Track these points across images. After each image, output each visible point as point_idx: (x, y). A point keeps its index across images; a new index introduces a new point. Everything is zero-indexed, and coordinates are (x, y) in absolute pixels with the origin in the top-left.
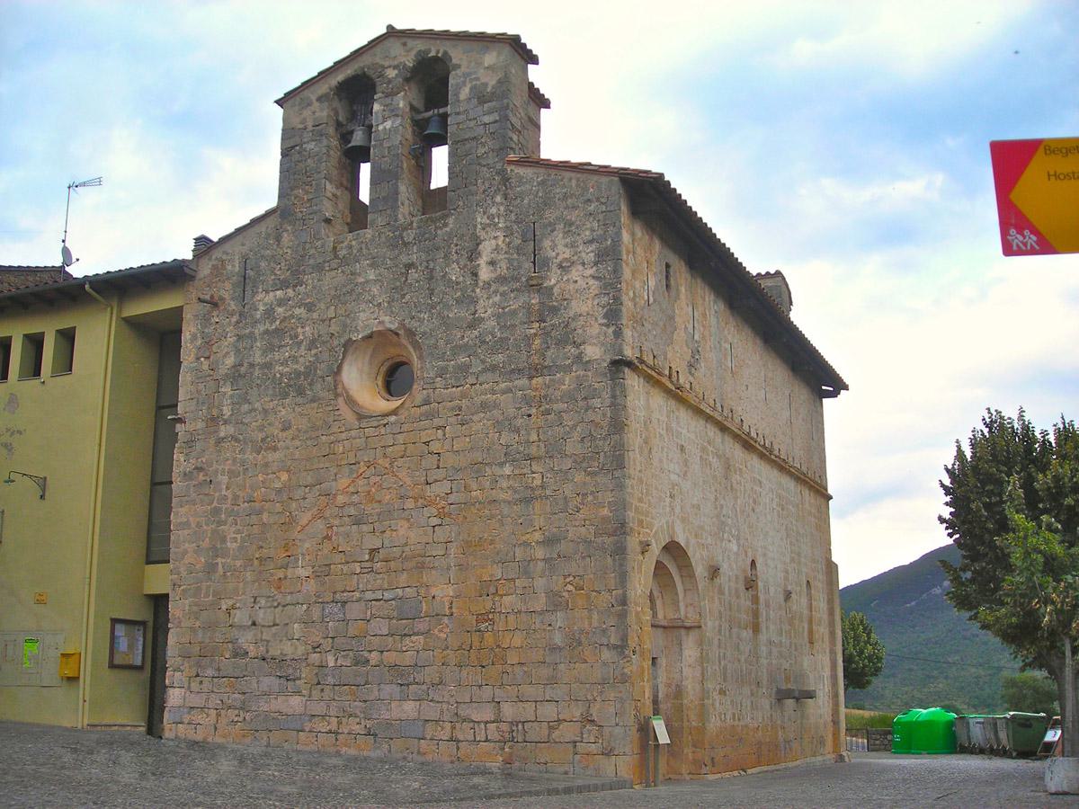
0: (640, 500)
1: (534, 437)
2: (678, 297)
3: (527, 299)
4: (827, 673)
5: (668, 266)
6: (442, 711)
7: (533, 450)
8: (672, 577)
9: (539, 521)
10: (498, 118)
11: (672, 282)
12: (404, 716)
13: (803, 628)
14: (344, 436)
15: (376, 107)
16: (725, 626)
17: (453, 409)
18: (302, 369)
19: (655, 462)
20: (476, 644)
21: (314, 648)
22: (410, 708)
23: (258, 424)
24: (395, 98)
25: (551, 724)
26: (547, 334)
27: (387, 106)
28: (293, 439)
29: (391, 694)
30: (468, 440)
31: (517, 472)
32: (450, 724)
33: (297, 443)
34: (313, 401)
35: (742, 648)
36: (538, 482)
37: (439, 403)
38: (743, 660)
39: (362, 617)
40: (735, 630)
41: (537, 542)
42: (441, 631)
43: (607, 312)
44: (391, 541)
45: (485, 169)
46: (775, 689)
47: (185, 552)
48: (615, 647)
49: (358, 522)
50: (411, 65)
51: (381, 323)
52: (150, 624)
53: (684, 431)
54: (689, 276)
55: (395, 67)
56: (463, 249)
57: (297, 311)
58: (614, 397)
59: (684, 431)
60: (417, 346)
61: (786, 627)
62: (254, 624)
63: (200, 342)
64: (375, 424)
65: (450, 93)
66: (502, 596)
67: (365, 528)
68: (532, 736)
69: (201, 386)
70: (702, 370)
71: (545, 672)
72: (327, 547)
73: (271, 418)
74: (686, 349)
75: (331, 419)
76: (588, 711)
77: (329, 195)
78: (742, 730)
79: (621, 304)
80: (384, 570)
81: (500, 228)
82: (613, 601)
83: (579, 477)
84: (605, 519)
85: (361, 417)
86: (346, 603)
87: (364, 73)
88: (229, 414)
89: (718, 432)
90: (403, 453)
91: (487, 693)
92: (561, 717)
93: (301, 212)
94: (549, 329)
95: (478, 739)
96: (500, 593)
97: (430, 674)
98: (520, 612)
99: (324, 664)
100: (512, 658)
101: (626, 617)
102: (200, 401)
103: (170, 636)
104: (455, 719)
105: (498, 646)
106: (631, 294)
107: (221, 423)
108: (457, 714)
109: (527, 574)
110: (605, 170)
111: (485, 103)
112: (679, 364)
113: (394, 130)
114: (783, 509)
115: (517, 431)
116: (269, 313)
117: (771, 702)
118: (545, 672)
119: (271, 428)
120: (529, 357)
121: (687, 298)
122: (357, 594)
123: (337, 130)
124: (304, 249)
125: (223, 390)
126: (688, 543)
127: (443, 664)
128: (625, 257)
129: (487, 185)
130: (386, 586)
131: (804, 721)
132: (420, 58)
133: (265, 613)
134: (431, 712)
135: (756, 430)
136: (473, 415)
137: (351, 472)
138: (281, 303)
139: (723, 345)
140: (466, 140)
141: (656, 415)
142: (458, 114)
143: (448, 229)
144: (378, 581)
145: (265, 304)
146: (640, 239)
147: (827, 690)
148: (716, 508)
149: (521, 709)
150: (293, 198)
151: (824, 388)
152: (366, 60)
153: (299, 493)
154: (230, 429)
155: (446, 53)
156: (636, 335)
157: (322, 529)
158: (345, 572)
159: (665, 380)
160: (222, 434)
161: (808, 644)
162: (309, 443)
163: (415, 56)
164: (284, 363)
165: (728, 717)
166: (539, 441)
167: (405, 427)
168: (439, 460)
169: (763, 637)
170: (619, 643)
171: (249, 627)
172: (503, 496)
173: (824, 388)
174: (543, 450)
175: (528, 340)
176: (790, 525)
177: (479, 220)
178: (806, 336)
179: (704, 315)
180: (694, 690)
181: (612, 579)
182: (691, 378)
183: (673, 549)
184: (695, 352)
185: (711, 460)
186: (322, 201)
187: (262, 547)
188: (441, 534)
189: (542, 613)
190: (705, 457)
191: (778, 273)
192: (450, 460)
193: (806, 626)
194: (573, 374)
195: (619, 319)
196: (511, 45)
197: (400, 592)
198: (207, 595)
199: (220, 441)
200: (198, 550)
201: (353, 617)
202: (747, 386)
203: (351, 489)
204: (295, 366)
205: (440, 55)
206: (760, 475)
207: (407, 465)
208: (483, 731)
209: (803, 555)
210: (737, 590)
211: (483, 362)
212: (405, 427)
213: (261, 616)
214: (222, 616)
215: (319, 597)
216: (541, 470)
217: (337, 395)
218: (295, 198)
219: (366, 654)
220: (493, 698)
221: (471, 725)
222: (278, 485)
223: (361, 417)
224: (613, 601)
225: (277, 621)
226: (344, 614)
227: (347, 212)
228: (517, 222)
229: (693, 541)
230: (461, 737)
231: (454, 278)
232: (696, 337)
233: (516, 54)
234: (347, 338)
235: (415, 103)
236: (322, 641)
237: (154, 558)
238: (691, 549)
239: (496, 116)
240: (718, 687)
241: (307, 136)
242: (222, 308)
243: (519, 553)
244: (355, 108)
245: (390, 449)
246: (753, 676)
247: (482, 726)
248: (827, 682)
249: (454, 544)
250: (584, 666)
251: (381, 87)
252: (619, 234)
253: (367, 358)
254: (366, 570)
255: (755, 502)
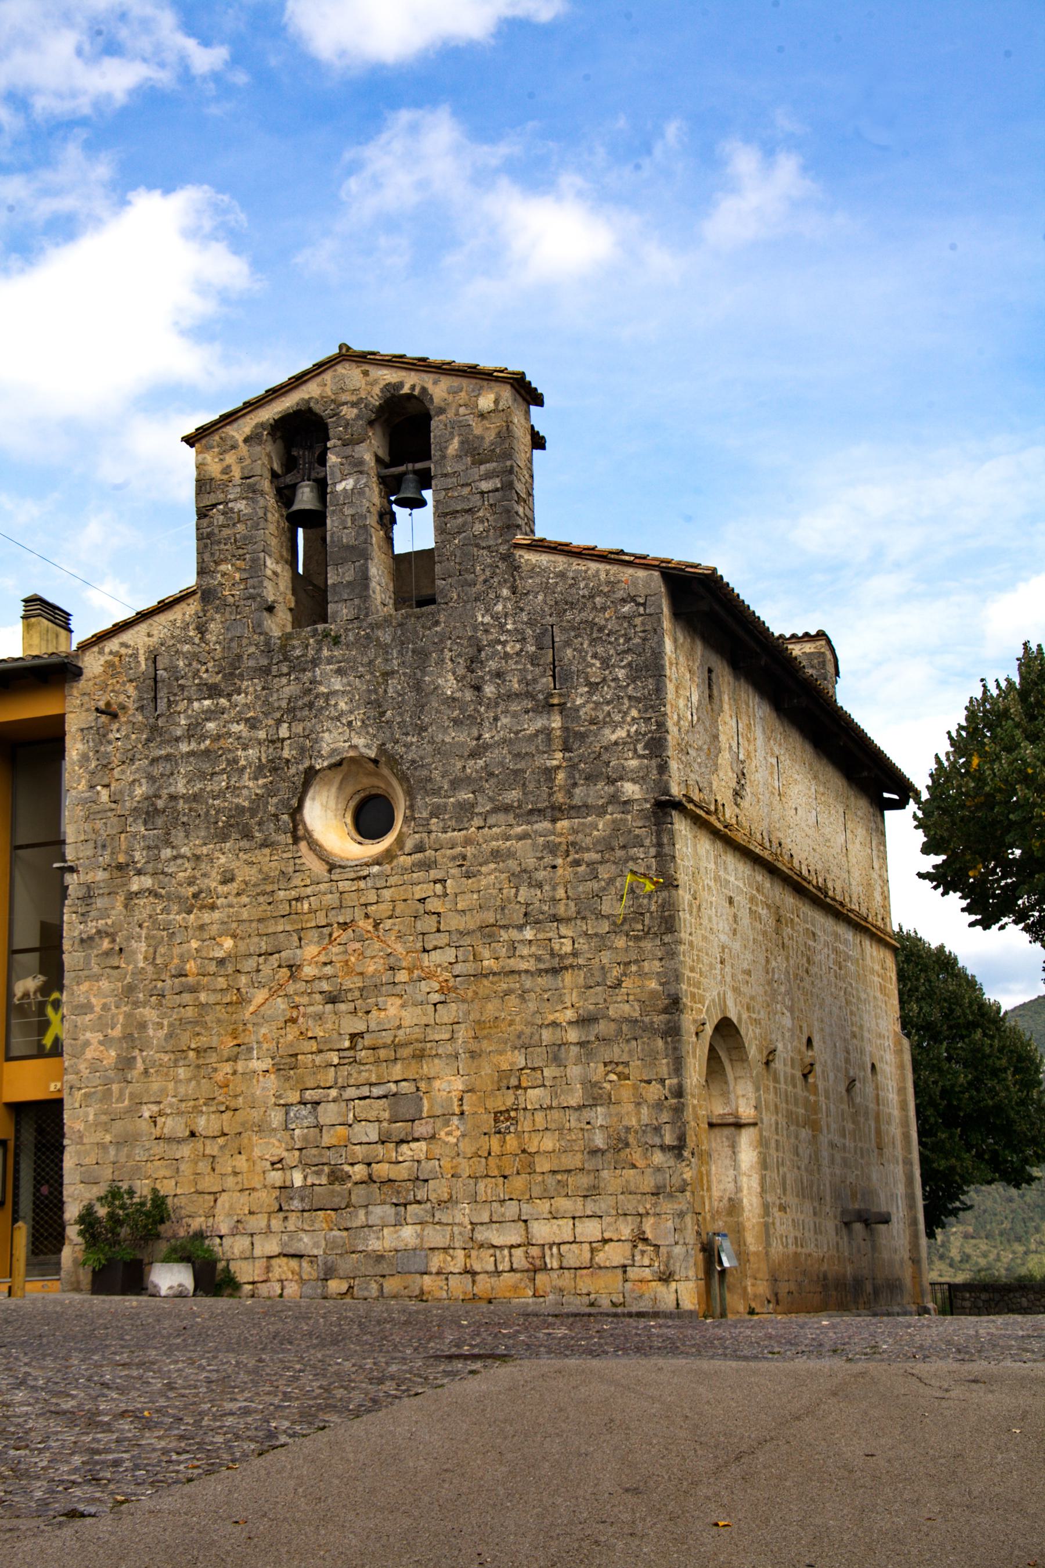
0: (692, 970)
1: (561, 893)
2: (721, 710)
3: (546, 722)
4: (901, 1189)
5: (710, 671)
6: (452, 1236)
7: (561, 910)
8: (721, 1062)
9: (572, 997)
10: (499, 486)
11: (715, 692)
12: (401, 1246)
13: (870, 1127)
14: (309, 891)
15: (332, 459)
16: (782, 1121)
17: (454, 858)
18: (246, 804)
19: (705, 921)
20: (496, 1149)
21: (273, 1164)
22: (408, 1234)
23: (187, 874)
24: (357, 448)
25: (594, 1245)
26: (573, 767)
27: (347, 458)
28: (238, 894)
29: (382, 1218)
30: (475, 896)
31: (540, 936)
32: (463, 1252)
33: (245, 899)
34: (264, 844)
35: (800, 1150)
36: (568, 948)
37: (436, 850)
38: (803, 1167)
39: (340, 1120)
40: (792, 1128)
41: (570, 1023)
42: (448, 1134)
43: (649, 740)
44: (378, 1023)
45: (485, 552)
46: (839, 1210)
47: (87, 1043)
48: (671, 1148)
49: (332, 999)
50: (377, 403)
51: (354, 747)
52: (11, 1145)
53: (732, 879)
54: (732, 680)
55: (354, 405)
56: (460, 655)
57: (235, 728)
58: (659, 845)
59: (732, 879)
60: (403, 779)
61: (850, 1126)
62: (193, 1134)
63: (93, 766)
64: (352, 875)
65: (433, 446)
66: (526, 1089)
67: (342, 1007)
68: (571, 1261)
69: (99, 824)
70: (748, 798)
71: (584, 1181)
72: (292, 1033)
73: (204, 866)
74: (730, 774)
75: (291, 869)
76: (640, 1227)
77: (269, 573)
78: (806, 1260)
79: (667, 732)
80: (371, 1059)
81: (508, 631)
82: (668, 1095)
83: (620, 942)
84: (653, 994)
85: (332, 867)
86: (318, 1103)
87: (310, 410)
88: (143, 861)
89: (767, 875)
90: (390, 913)
91: (511, 1210)
92: (607, 1235)
93: (233, 595)
94: (576, 760)
95: (500, 1268)
96: (524, 1085)
97: (438, 1189)
98: (550, 1108)
99: (288, 1184)
100: (543, 1165)
101: (682, 1112)
102: (99, 843)
103: (67, 1157)
104: (470, 1245)
105: (524, 1151)
106: (675, 717)
107: (132, 873)
108: (472, 1238)
109: (557, 1060)
110: (642, 561)
111: (481, 464)
112: (724, 796)
113: (358, 492)
114: (840, 969)
115: (540, 886)
116: (193, 731)
117: (836, 1226)
118: (584, 1181)
119: (206, 881)
120: (550, 795)
121: (730, 709)
122: (334, 1093)
123: (271, 482)
124: (240, 646)
125: (132, 829)
126: (740, 1019)
127: (452, 1176)
128: (668, 673)
129: (488, 573)
130: (374, 1080)
131: (876, 1255)
132: (388, 395)
133: (208, 1120)
134: (436, 1237)
135: (808, 866)
136: (481, 865)
137: (321, 937)
138: (210, 715)
139: (770, 760)
140: (457, 512)
141: (704, 864)
142: (446, 475)
143: (438, 629)
144: (363, 1074)
145: (189, 717)
146: (682, 645)
147: (901, 1215)
148: (767, 973)
149: (555, 1227)
150: (219, 575)
151: (886, 795)
152: (311, 390)
153: (250, 964)
154: (147, 882)
155: (424, 390)
156: (681, 767)
157: (284, 1010)
158: (317, 1063)
159: (712, 819)
160: (135, 888)
161: (876, 1150)
162: (261, 899)
163: (382, 390)
164: (220, 795)
165: (790, 1241)
166: (568, 898)
167: (392, 880)
168: (439, 922)
169: (824, 1139)
170: (675, 1143)
171: (184, 1140)
172: (524, 966)
173: (886, 795)
174: (573, 909)
175: (549, 773)
176: (849, 989)
177: (480, 619)
178: (869, 735)
179: (749, 726)
180: (751, 1205)
181: (664, 1066)
182: (737, 810)
183: (726, 1028)
184: (740, 776)
185: (761, 911)
186: (261, 582)
187: (198, 1034)
188: (447, 1014)
189: (579, 1108)
190: (754, 908)
191: (821, 635)
192: (454, 922)
193: (873, 1124)
194: (608, 817)
195: (664, 750)
196: (512, 385)
197: (393, 1087)
198: (121, 1099)
199: (131, 896)
200: (106, 1041)
201: (328, 1121)
202: (796, 809)
203: (323, 958)
204: (236, 800)
205: (416, 393)
206: (813, 925)
207: (397, 928)
208: (507, 1259)
209: (865, 1029)
210: (793, 1077)
211: (491, 799)
212: (392, 880)
213: (201, 1123)
214: (144, 1125)
215: (279, 1097)
216: (571, 934)
217: (296, 840)
218: (222, 576)
219: (347, 1168)
220: (520, 1215)
221: (491, 1251)
222: (220, 954)
223: (332, 867)
224: (668, 1095)
225: (226, 1131)
226: (316, 1118)
227: (289, 592)
228: (531, 623)
229: (745, 1016)
230: (477, 1267)
231: (449, 693)
232: (741, 757)
233: (518, 396)
234: (307, 764)
235: (381, 453)
236: (285, 1154)
237: (15, 1053)
238: (743, 1025)
239: (497, 483)
240: (778, 1202)
241: (233, 493)
242: (123, 719)
243: (546, 1035)
244: (295, 453)
245: (374, 907)
246: (815, 1189)
247: (506, 1252)
248: (901, 1203)
249: (463, 1026)
250: (632, 1172)
251: (336, 431)
252: (661, 643)
253: (334, 790)
254: (347, 1061)
255: (808, 961)
